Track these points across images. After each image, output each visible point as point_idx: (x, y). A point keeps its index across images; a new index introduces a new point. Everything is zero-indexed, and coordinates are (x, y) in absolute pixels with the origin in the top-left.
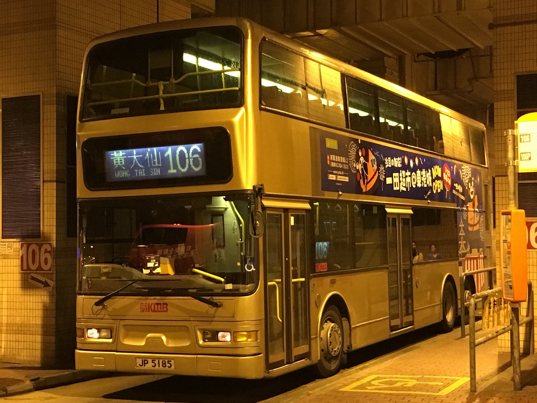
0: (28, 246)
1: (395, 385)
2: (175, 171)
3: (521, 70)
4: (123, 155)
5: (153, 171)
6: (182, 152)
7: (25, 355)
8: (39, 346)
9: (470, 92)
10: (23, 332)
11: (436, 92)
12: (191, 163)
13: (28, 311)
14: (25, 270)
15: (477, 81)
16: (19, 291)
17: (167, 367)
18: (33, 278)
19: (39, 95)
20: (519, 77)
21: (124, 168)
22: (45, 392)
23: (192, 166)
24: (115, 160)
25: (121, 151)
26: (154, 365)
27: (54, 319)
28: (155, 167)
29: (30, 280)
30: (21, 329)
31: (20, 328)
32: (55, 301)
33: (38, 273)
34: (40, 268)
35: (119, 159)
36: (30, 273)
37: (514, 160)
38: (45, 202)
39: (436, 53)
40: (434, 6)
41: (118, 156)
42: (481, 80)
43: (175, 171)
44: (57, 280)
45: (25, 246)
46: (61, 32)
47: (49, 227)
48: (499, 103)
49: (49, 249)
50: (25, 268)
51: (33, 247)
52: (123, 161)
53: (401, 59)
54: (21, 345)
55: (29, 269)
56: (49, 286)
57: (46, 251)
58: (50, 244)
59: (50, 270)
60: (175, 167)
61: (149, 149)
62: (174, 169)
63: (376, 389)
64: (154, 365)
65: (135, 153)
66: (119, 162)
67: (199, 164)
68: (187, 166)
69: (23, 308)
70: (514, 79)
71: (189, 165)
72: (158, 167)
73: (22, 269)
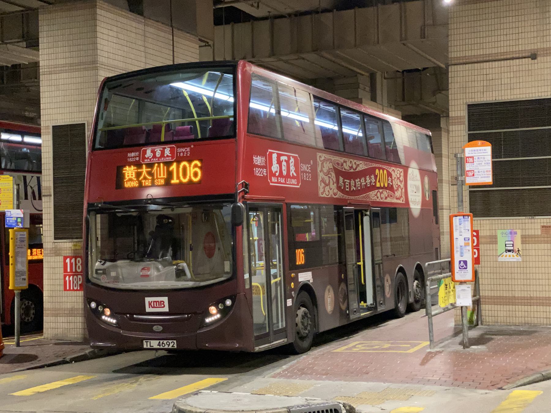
3: (471, 100)
4: (134, 169)
9: (434, 103)
11: (403, 103)
12: (192, 175)
15: (440, 93)
19: (85, 124)
20: (469, 106)
28: (160, 178)
30: (71, 312)
37: (462, 176)
43: (178, 181)
48: (454, 126)
52: (134, 174)
53: (372, 77)
54: (72, 326)
60: (178, 177)
66: (130, 175)
68: (188, 178)
70: (465, 108)
71: (190, 177)
72: (162, 178)
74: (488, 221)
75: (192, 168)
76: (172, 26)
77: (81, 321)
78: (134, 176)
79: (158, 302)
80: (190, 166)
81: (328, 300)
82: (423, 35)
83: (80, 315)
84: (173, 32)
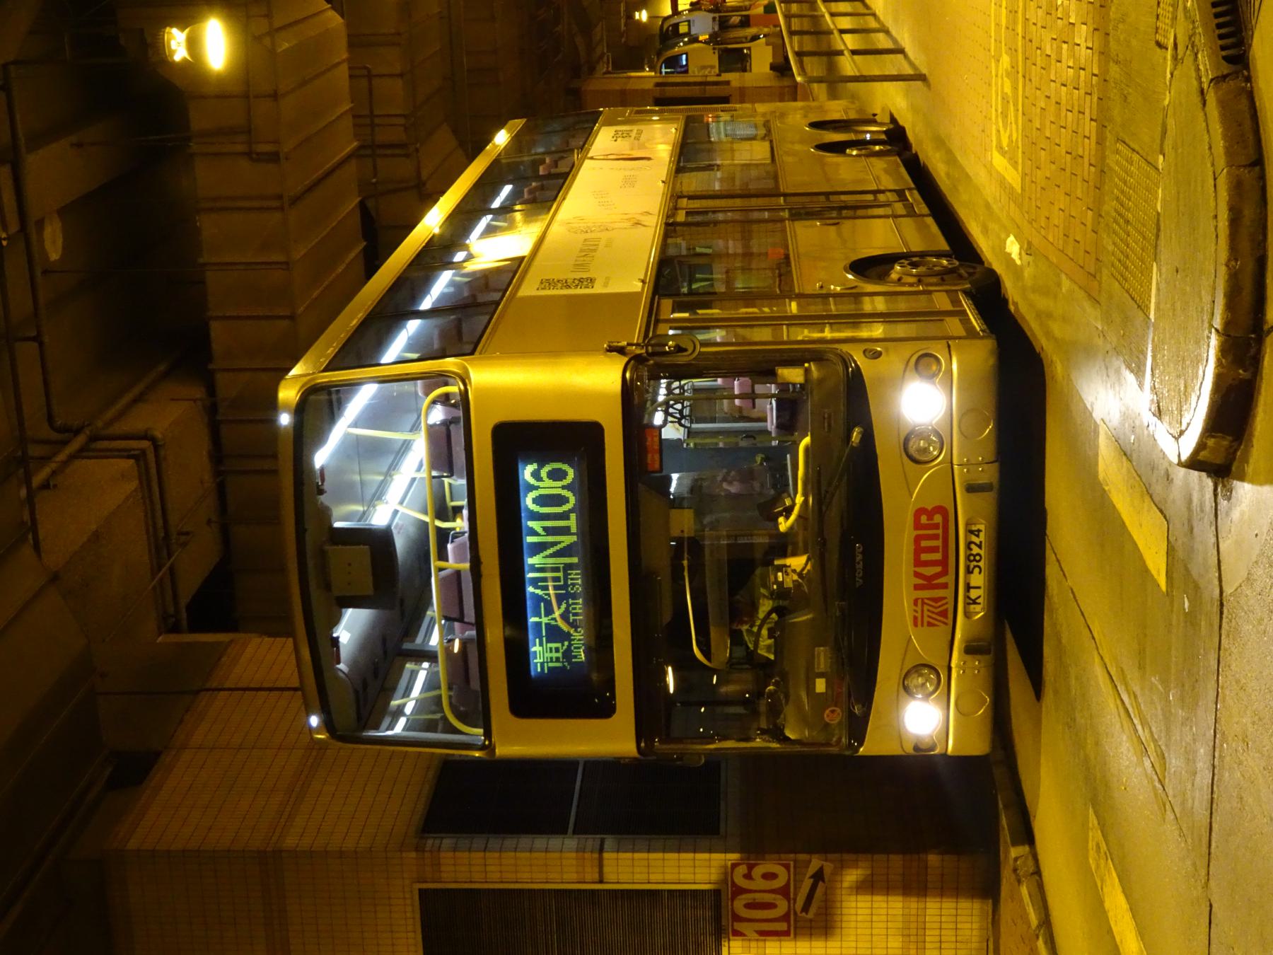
0: (737, 918)
1: (1010, 94)
2: (573, 516)
4: (541, 644)
5: (574, 585)
6: (535, 501)
7: (969, 926)
8: (949, 905)
10: (921, 932)
12: (559, 484)
13: (875, 918)
14: (789, 927)
15: (424, 184)
16: (833, 946)
17: (982, 552)
18: (806, 908)
19: (422, 892)
21: (566, 643)
22: (1037, 796)
23: (565, 482)
24: (551, 665)
25: (533, 649)
26: (977, 570)
27: (892, 856)
29: (811, 915)
30: (914, 934)
31: (913, 938)
32: (853, 856)
33: (796, 894)
34: (784, 892)
35: (548, 655)
36: (795, 913)
38: (644, 877)
39: (365, 237)
40: (269, 209)
41: (541, 655)
42: (425, 174)
43: (573, 516)
44: (810, 852)
45: (738, 926)
46: (290, 842)
47: (697, 870)
49: (742, 869)
50: (782, 926)
51: (739, 904)
52: (554, 645)
54: (949, 935)
55: (785, 918)
56: (821, 869)
57: (748, 876)
58: (734, 866)
59: (787, 867)
60: (564, 516)
61: (530, 589)
62: (568, 519)
63: (1016, 105)
64: (977, 570)
65: (537, 619)
66: (554, 655)
67: (560, 469)
69: (868, 932)
71: (563, 487)
73: (787, 933)
74: (668, 877)
75: (540, 484)
76: (198, 692)
77: (938, 905)
78: (559, 645)
79: (917, 539)
80: (537, 488)
81: (879, 235)
82: (274, 157)
83: (921, 905)
84: (214, 690)
